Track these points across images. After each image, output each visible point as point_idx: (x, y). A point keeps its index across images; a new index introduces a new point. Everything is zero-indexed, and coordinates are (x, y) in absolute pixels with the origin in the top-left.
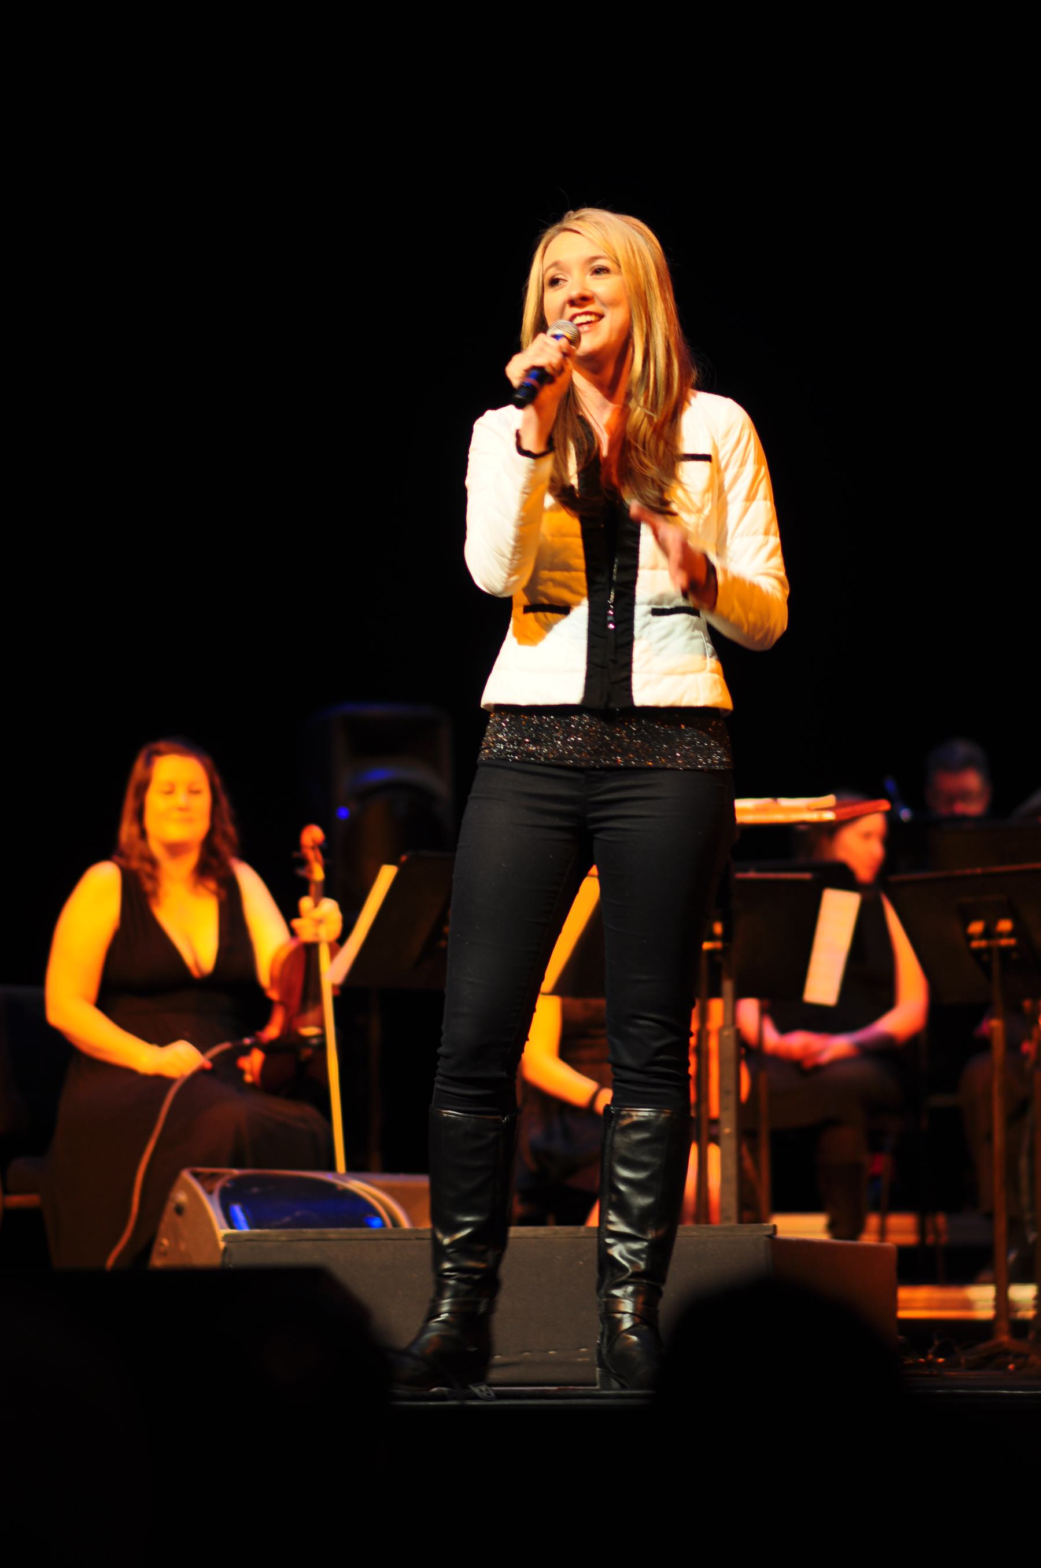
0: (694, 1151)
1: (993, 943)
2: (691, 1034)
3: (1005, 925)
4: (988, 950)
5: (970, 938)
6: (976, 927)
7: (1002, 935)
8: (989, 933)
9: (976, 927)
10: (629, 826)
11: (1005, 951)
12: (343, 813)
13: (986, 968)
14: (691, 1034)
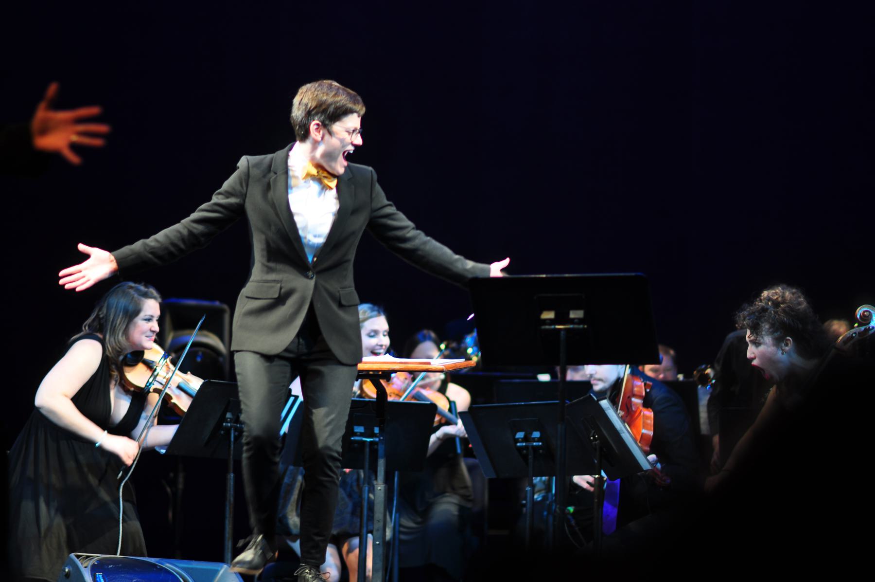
0: (94, 110)
1: (530, 444)
2: (712, 385)
3: (536, 434)
4: (526, 447)
5: (517, 441)
6: (520, 435)
7: (534, 440)
8: (526, 439)
9: (520, 435)
10: (631, 439)
11: (535, 448)
12: (709, 371)
13: (525, 458)
14: (712, 385)
